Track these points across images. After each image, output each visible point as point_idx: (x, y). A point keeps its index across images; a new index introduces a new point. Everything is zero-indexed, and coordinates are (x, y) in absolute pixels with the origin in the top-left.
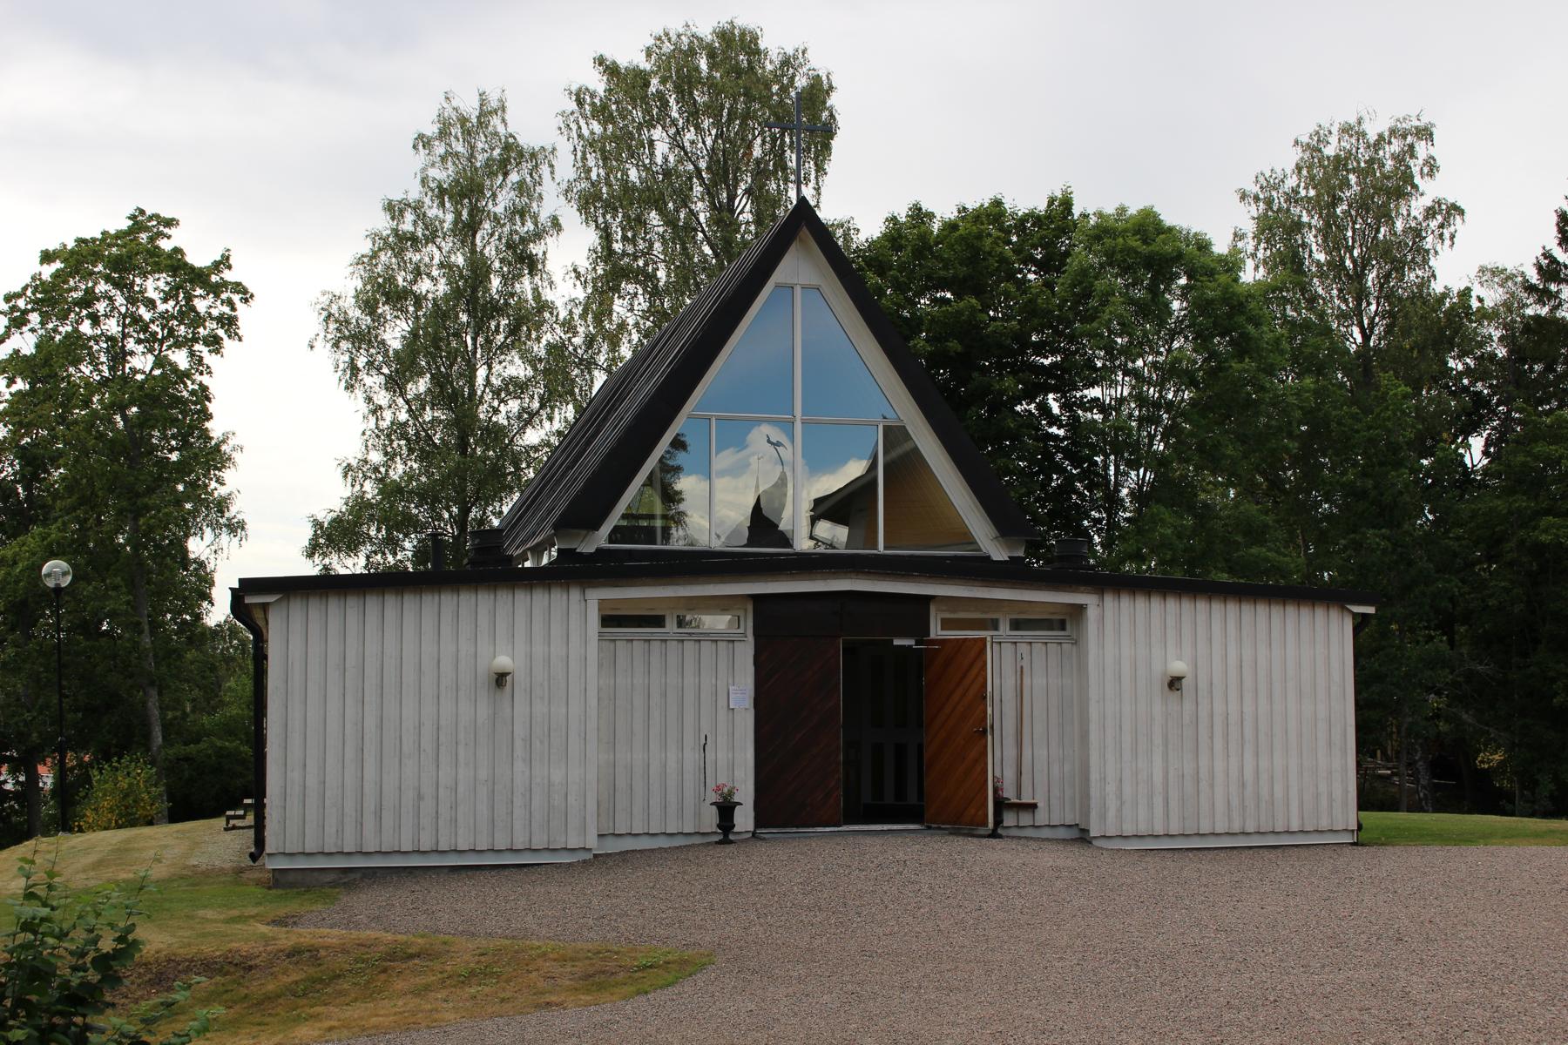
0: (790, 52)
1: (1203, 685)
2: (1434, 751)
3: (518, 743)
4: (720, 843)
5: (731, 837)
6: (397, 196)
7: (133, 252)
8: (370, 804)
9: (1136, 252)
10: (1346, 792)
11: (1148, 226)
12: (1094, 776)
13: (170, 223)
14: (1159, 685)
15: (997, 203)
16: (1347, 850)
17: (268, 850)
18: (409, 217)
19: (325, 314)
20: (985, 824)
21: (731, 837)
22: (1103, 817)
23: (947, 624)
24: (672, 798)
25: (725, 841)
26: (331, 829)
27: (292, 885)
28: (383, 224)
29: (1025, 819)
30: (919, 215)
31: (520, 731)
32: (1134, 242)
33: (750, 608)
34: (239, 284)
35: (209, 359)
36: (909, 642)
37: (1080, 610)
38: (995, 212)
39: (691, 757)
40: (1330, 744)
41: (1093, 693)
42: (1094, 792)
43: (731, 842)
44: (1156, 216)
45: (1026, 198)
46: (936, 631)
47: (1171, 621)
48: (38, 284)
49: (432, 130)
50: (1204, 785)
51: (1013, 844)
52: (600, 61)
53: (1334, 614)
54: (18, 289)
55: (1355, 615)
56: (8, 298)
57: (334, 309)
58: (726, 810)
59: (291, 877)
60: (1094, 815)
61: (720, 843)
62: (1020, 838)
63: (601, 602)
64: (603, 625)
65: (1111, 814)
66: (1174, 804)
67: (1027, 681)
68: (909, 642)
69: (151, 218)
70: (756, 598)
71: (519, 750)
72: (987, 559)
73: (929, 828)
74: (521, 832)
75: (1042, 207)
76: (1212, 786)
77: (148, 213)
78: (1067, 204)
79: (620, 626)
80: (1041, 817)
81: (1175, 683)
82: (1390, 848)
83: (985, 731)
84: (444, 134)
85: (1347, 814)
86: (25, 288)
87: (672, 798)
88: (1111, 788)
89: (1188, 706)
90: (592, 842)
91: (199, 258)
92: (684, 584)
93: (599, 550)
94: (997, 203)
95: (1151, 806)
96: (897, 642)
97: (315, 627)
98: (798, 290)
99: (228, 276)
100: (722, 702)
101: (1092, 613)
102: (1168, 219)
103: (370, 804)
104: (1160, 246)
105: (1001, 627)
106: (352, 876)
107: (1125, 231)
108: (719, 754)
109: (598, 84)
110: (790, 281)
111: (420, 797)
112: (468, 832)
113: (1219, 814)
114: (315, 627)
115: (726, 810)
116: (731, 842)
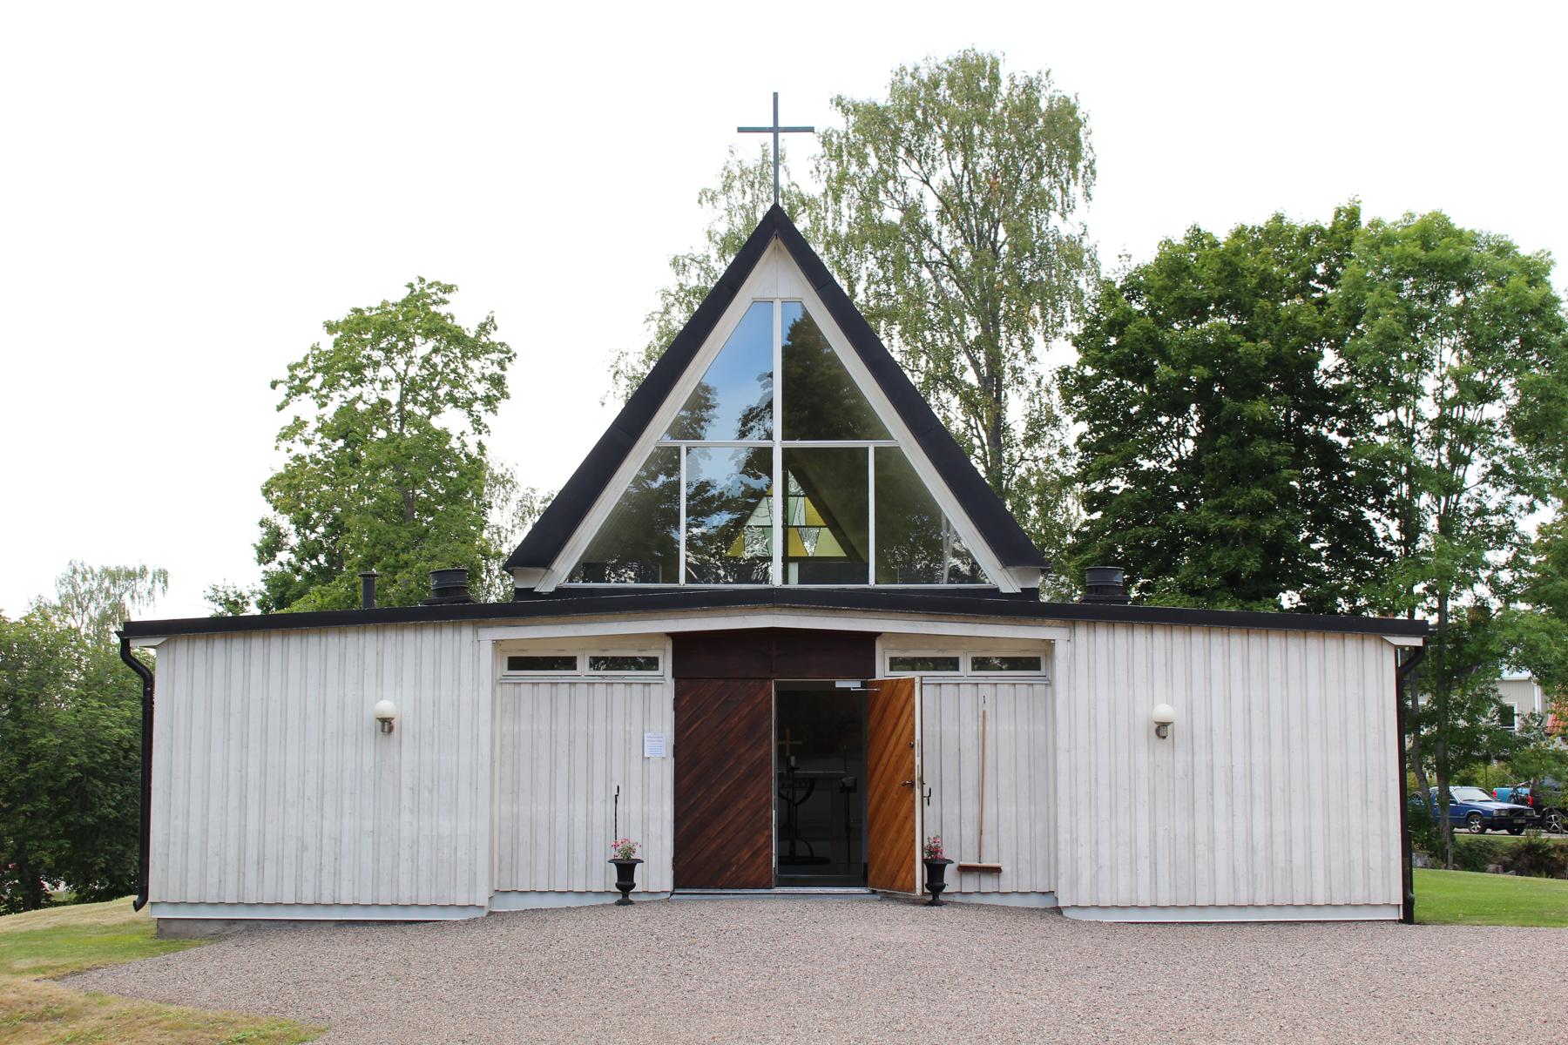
0: (1033, 75)
1: (1200, 729)
2: (1494, 811)
3: (406, 793)
4: (619, 903)
5: (631, 897)
6: (682, 251)
7: (417, 316)
8: (252, 854)
9: (1414, 260)
10: (1376, 859)
11: (1432, 231)
12: (1064, 837)
13: (449, 289)
14: (1144, 731)
15: (1279, 218)
16: (1391, 927)
17: (150, 899)
18: (694, 270)
19: (613, 371)
20: (913, 889)
21: (941, 898)
22: (1074, 883)
23: (895, 664)
24: (580, 855)
25: (626, 902)
26: (212, 880)
27: (176, 935)
28: (671, 281)
29: (988, 883)
30: (1197, 237)
31: (407, 779)
32: (1415, 250)
33: (669, 647)
34: (503, 344)
35: (487, 418)
36: (854, 685)
37: (1049, 645)
38: (1276, 232)
39: (602, 809)
40: (1366, 802)
41: (1062, 742)
42: (1064, 855)
43: (631, 903)
44: (1445, 219)
45: (1312, 210)
46: (882, 671)
47: (1159, 658)
48: (317, 353)
49: (716, 185)
50: (1201, 849)
51: (971, 916)
52: (839, 102)
53: (1371, 646)
54: (301, 360)
55: (1396, 647)
56: (292, 368)
57: (622, 366)
58: (626, 870)
59: (174, 927)
60: (1063, 881)
61: (619, 903)
62: (980, 906)
63: (497, 643)
64: (510, 668)
65: (1085, 881)
66: (1163, 869)
67: (990, 727)
68: (854, 685)
69: (430, 286)
70: (675, 637)
71: (406, 801)
72: (995, 592)
73: (874, 892)
74: (406, 887)
75: (1326, 222)
76: (1212, 850)
77: (428, 281)
78: (1354, 214)
79: (553, 669)
80: (1007, 882)
81: (1161, 729)
82: (1462, 928)
83: (913, 784)
84: (727, 188)
85: (669, 886)
86: (306, 358)
87: (580, 855)
88: (1084, 851)
89: (1181, 756)
90: (482, 900)
91: (468, 323)
92: (500, 625)
93: (560, 591)
94: (1279, 218)
95: (1134, 872)
96: (840, 684)
97: (200, 671)
98: (777, 305)
99: (495, 337)
100: (636, 750)
101: (1061, 650)
102: (1460, 222)
103: (252, 854)
104: (1448, 252)
105: (579, 663)
106: (236, 927)
107: (1405, 237)
108: (632, 807)
109: (839, 123)
110: (768, 295)
111: (304, 848)
112: (353, 886)
113: (1220, 882)
114: (200, 671)
115: (626, 870)
116: (631, 903)
